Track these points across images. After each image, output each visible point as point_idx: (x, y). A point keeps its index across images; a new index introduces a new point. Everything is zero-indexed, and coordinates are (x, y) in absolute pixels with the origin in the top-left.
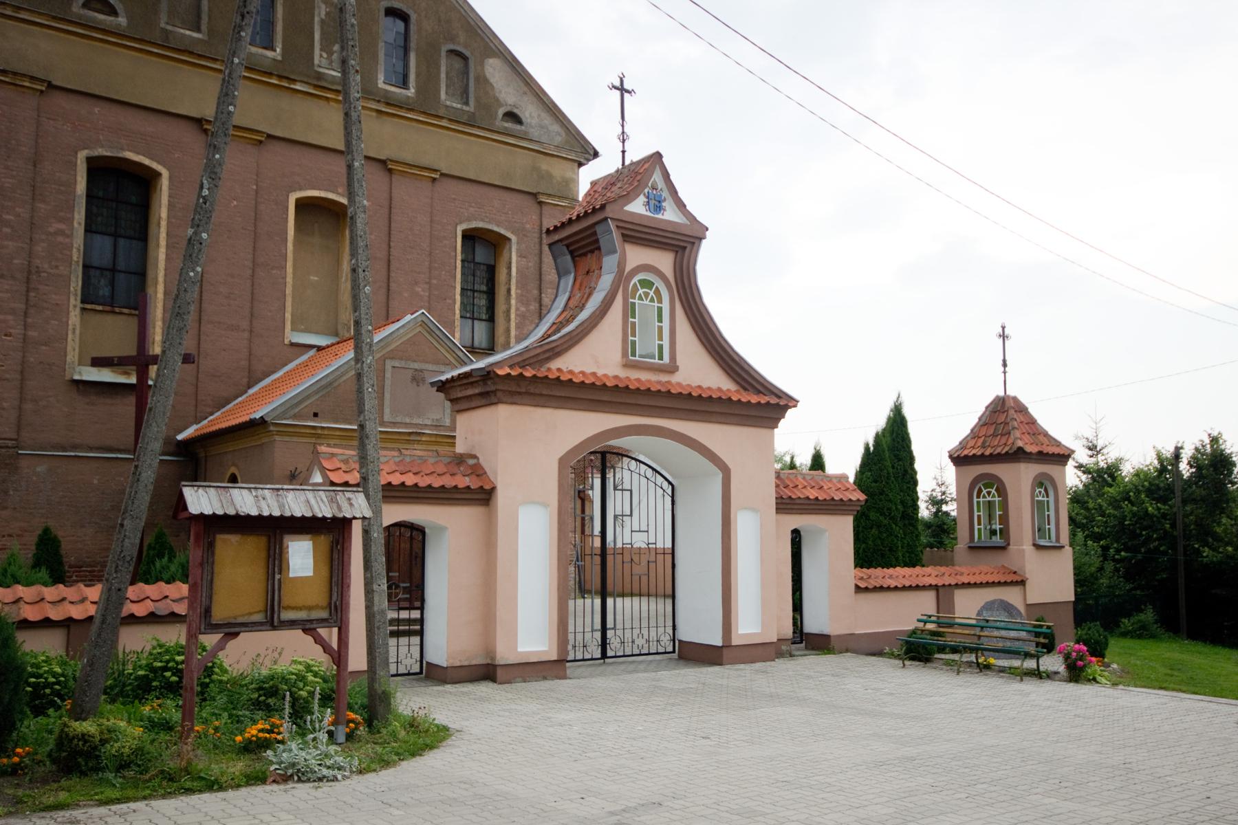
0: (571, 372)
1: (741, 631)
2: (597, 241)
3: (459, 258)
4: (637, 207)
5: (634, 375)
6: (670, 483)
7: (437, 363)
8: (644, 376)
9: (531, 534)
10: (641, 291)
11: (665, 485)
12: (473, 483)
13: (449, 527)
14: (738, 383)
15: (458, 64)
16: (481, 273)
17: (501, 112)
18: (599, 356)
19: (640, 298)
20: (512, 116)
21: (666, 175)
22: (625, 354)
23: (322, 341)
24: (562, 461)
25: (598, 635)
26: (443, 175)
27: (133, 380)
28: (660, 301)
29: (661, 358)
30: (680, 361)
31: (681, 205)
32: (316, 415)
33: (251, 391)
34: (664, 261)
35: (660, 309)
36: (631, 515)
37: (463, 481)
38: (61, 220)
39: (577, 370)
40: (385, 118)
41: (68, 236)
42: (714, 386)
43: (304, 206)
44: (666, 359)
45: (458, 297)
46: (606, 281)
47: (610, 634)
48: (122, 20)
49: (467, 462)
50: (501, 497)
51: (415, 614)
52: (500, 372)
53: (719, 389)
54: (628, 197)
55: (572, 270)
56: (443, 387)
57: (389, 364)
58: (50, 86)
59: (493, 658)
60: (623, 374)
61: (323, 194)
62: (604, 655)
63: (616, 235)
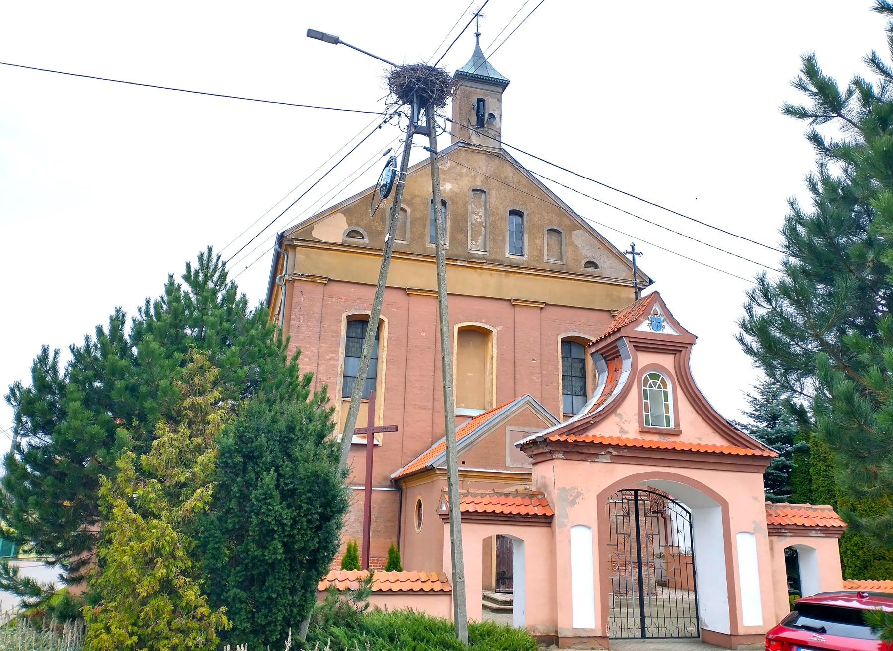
0: (602, 437)
1: (592, 626)
2: (618, 351)
3: (560, 356)
4: (644, 327)
5: (649, 438)
6: (687, 511)
7: (538, 427)
8: (656, 439)
9: (581, 548)
10: (651, 381)
11: (684, 513)
12: (539, 511)
13: (529, 537)
14: (729, 441)
15: (555, 237)
16: (577, 366)
17: (584, 262)
18: (623, 427)
19: (651, 386)
20: (591, 264)
21: (663, 305)
22: (641, 424)
23: (475, 413)
24: (599, 497)
25: (638, 621)
26: (547, 305)
27: (364, 441)
28: (665, 386)
29: (668, 425)
30: (683, 427)
31: (675, 324)
32: (464, 463)
33: (433, 447)
34: (667, 361)
35: (666, 393)
36: (659, 535)
37: (532, 510)
38: (333, 352)
39: (606, 436)
40: (511, 275)
41: (336, 360)
42: (710, 444)
43: (463, 331)
44: (672, 425)
45: (560, 381)
46: (624, 377)
47: (647, 620)
48: (366, 241)
49: (538, 496)
50: (556, 520)
51: (507, 598)
52: (553, 439)
53: (714, 446)
54: (636, 322)
55: (606, 369)
56: (523, 447)
57: (508, 428)
58: (330, 279)
59: (556, 632)
60: (639, 437)
61: (470, 324)
62: (643, 636)
63: (629, 347)
